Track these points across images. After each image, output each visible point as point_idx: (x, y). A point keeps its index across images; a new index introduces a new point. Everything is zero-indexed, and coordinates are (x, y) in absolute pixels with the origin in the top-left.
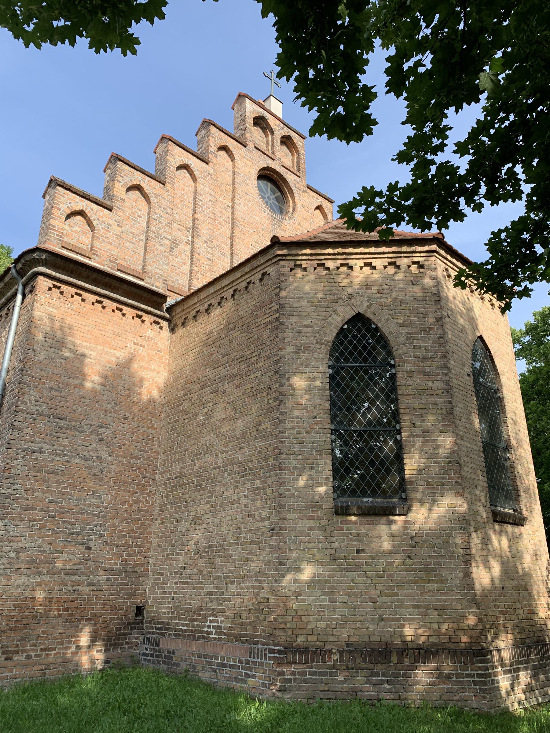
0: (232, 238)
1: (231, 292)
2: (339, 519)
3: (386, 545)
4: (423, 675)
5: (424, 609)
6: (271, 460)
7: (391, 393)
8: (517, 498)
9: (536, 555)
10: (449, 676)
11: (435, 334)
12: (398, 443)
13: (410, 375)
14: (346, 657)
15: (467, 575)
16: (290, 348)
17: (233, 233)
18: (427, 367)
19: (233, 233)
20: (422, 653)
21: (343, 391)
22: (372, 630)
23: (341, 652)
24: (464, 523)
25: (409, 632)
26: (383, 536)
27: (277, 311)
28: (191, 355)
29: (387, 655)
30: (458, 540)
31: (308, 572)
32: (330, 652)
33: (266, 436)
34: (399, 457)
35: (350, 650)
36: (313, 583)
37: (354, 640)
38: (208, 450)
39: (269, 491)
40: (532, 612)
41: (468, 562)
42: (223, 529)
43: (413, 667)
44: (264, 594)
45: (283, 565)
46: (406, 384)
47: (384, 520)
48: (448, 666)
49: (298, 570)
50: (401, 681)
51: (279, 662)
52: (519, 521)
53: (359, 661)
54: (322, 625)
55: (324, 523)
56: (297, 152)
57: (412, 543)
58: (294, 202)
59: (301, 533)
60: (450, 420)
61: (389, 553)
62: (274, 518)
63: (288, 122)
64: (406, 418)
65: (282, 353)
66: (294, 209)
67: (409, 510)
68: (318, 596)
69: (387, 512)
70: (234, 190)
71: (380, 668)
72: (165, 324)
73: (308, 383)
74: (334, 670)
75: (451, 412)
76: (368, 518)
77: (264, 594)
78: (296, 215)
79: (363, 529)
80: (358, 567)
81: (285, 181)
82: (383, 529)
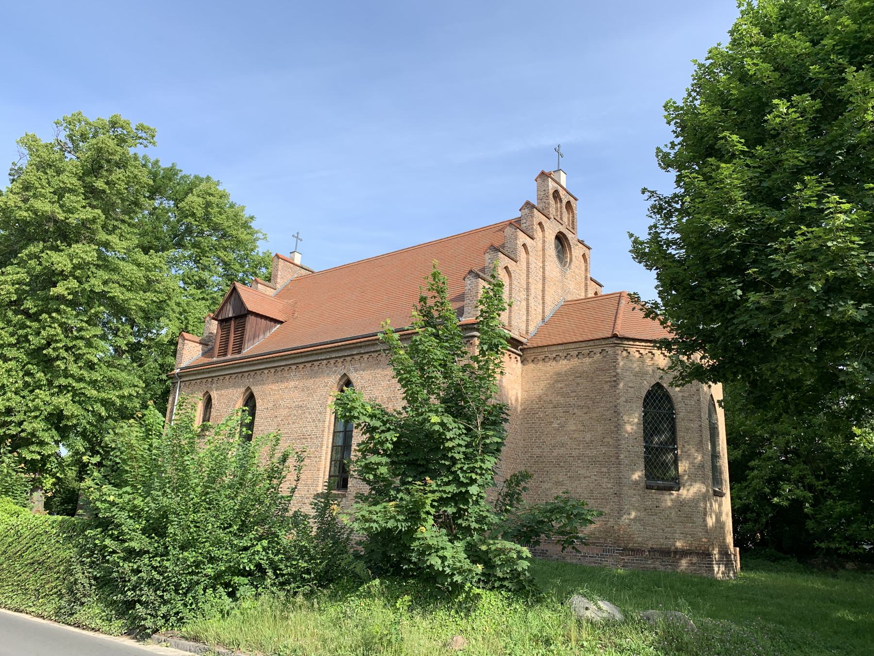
0: (543, 291)
1: (576, 353)
2: (648, 491)
3: (669, 504)
4: (684, 563)
5: (685, 534)
6: (613, 459)
7: (673, 430)
8: (722, 484)
9: (727, 514)
10: (695, 564)
11: (695, 398)
12: (676, 455)
13: (683, 420)
14: (652, 553)
15: (705, 520)
16: (623, 399)
17: (544, 287)
18: (691, 416)
19: (544, 287)
20: (684, 553)
21: (650, 427)
22: (659, 542)
23: (649, 551)
24: (705, 497)
25: (679, 544)
26: (668, 499)
27: (615, 376)
28: (543, 384)
29: (669, 554)
30: (702, 505)
31: (633, 514)
32: (644, 551)
33: (608, 445)
34: (675, 462)
35: (652, 550)
36: (635, 519)
37: (654, 546)
38: (563, 445)
39: (612, 474)
40: (724, 539)
41: (705, 515)
42: (579, 490)
43: (680, 559)
44: (609, 524)
45: (620, 512)
46: (680, 425)
47: (667, 493)
48: (695, 560)
49: (629, 514)
50: (676, 563)
51: (622, 554)
52: (721, 495)
53: (657, 555)
54: (640, 539)
55: (641, 492)
56: (572, 212)
57: (681, 504)
58: (571, 255)
59: (630, 497)
60: (700, 446)
61: (670, 508)
62: (616, 489)
63: (568, 190)
64: (680, 443)
65: (618, 401)
66: (571, 260)
67: (678, 490)
68: (636, 527)
69: (670, 489)
70: (544, 255)
71: (665, 559)
72: (519, 358)
73: (632, 422)
74: (646, 559)
75: (701, 441)
76: (659, 492)
77: (609, 524)
78: (573, 266)
79: (659, 497)
80: (656, 514)
81: (566, 239)
82: (667, 497)
